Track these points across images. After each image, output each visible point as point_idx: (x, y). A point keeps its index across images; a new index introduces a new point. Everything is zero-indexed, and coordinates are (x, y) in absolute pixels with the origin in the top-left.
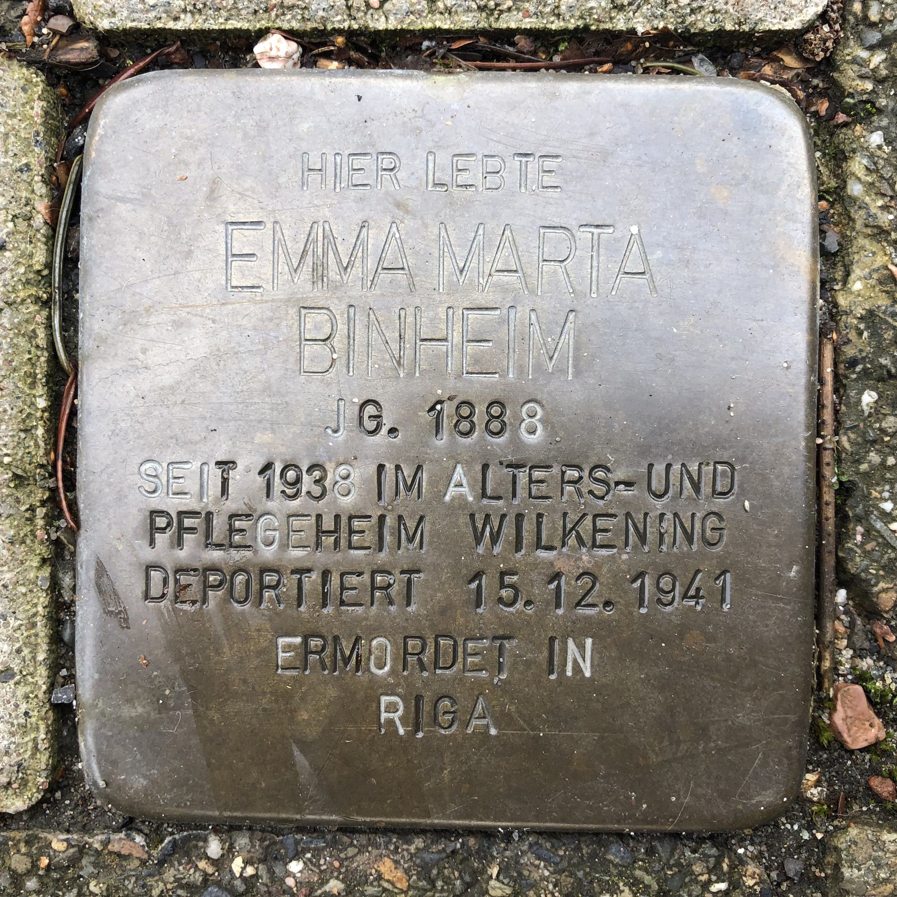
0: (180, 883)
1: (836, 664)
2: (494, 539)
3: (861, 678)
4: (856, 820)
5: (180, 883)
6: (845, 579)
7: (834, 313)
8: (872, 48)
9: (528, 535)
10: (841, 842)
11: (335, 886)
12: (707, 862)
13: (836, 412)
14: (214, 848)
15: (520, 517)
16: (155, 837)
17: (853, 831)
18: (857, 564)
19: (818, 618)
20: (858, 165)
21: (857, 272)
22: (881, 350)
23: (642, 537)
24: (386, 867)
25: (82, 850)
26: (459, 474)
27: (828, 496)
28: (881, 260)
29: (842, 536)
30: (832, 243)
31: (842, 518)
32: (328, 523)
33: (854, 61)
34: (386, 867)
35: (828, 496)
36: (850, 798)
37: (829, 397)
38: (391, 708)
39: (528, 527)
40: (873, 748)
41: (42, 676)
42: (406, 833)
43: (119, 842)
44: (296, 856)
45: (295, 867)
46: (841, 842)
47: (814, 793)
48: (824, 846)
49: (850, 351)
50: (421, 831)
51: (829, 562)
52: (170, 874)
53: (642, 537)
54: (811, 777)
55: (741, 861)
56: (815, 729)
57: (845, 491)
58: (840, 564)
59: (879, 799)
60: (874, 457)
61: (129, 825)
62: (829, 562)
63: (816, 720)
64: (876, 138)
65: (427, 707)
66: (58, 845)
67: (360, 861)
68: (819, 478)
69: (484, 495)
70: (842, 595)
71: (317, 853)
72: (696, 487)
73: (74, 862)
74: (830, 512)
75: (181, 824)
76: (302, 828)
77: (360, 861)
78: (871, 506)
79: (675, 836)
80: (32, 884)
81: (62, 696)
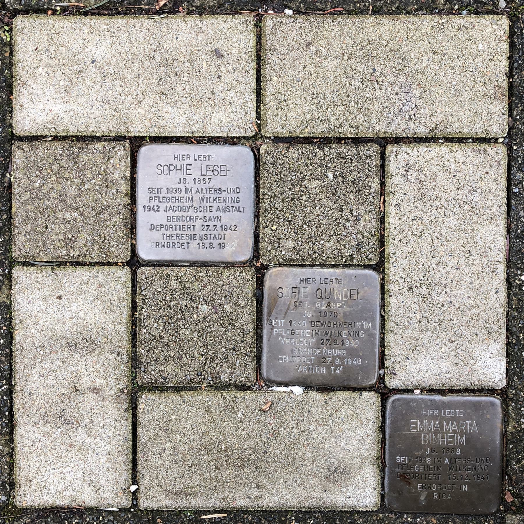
0: (400, 522)
1: (506, 488)
2: (452, 469)
3: (510, 490)
4: (509, 514)
5: (400, 522)
6: (507, 474)
7: (506, 431)
8: (513, 390)
9: (458, 469)
10: (506, 517)
11: (425, 522)
12: (380, 383)
13: (506, 448)
14: (405, 516)
15: (456, 466)
16: (396, 515)
17: (508, 515)
18: (509, 472)
19: (503, 481)
20: (510, 408)
21: (510, 425)
22: (513, 438)
23: (475, 469)
24: (433, 520)
25: (385, 516)
26: (447, 459)
27: (504, 462)
28: (514, 423)
29: (507, 468)
30: (506, 420)
31: (507, 465)
32: (177, 198)
33: (510, 392)
34: (433, 520)
35: (504, 462)
36: (508, 510)
37: (505, 445)
38: (436, 495)
39: (458, 468)
40: (512, 502)
41: (380, 489)
42: (436, 514)
43: (390, 515)
44: (419, 518)
45: (418, 519)
46: (506, 517)
47: (502, 509)
48: (503, 518)
49: (508, 438)
50: (438, 514)
51: (505, 472)
52: (398, 520)
53: (475, 469)
54: (501, 506)
55: (490, 520)
56: (502, 498)
57: (507, 460)
58: (506, 473)
59: (513, 510)
60: (512, 455)
61: (391, 512)
62: (505, 472)
63: (502, 497)
64: (513, 404)
65: (441, 495)
66: (381, 516)
67: (429, 519)
68: (503, 458)
69: (451, 463)
70: (507, 477)
71: (422, 517)
72: (484, 461)
73: (383, 518)
74: (505, 464)
75: (399, 513)
76: (420, 513)
77: (429, 519)
78: (512, 463)
79: (479, 515)
80: (376, 522)
81: (383, 492)
